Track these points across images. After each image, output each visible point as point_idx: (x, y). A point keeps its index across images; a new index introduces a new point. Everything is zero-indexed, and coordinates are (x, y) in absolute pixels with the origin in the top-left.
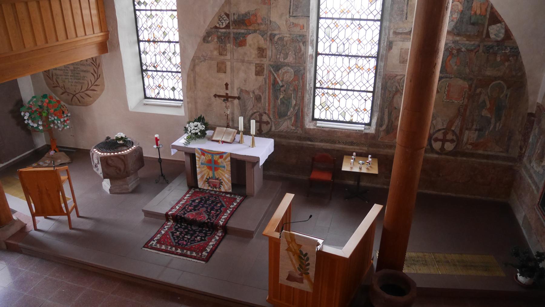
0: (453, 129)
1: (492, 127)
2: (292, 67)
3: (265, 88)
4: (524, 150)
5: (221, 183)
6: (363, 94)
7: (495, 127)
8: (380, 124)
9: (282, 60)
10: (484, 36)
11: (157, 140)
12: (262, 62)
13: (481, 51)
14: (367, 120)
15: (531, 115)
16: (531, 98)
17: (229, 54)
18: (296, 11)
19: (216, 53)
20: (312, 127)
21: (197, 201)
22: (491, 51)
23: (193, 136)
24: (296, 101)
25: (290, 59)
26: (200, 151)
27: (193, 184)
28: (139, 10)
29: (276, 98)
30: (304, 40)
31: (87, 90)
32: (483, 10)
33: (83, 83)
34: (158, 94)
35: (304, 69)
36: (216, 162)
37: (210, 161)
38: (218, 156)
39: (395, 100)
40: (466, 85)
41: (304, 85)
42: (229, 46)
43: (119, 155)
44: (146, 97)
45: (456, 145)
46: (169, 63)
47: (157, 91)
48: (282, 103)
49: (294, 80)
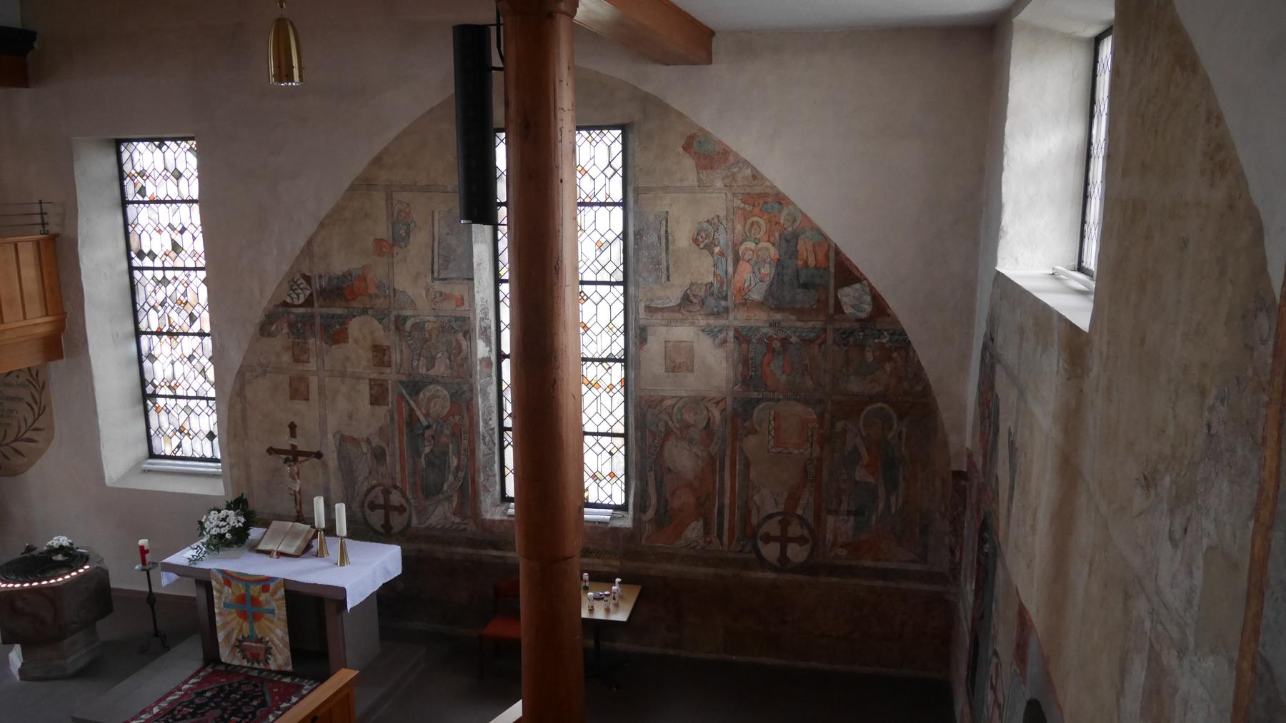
0: (799, 512)
1: (881, 506)
2: (445, 385)
4: (958, 554)
5: (268, 651)
6: (605, 441)
7: (888, 506)
8: (641, 507)
9: (423, 371)
10: (831, 311)
11: (143, 551)
12: (382, 377)
13: (830, 341)
14: (619, 499)
15: (958, 475)
16: (953, 439)
17: (313, 360)
18: (447, 268)
19: (286, 358)
20: (497, 517)
21: (208, 694)
22: (851, 340)
23: (215, 541)
24: (459, 460)
25: (441, 368)
26: (220, 576)
27: (211, 657)
28: (141, 269)
29: (416, 453)
31: (15, 440)
32: (821, 256)
33: (9, 425)
34: (179, 446)
35: (471, 391)
36: (255, 602)
37: (242, 599)
38: (259, 587)
39: (666, 454)
40: (811, 414)
41: (473, 425)
42: (313, 343)
43: (50, 587)
44: (152, 455)
45: (813, 550)
46: (201, 379)
47: (175, 441)
48: (430, 463)
49: (451, 414)
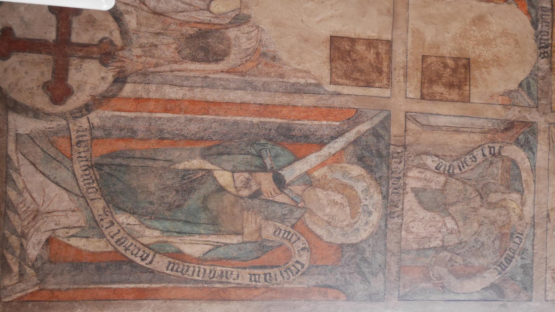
2: (381, 233)
3: (265, 87)
9: (414, 179)
12: (398, 75)
24: (200, 261)
25: (419, 223)
29: (217, 147)
30: (509, 292)
48: (189, 182)
49: (314, 242)
